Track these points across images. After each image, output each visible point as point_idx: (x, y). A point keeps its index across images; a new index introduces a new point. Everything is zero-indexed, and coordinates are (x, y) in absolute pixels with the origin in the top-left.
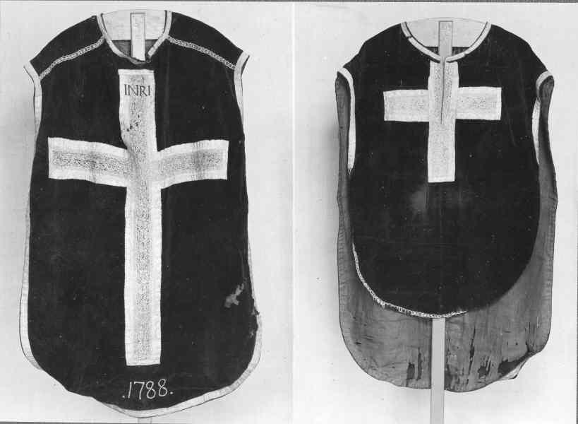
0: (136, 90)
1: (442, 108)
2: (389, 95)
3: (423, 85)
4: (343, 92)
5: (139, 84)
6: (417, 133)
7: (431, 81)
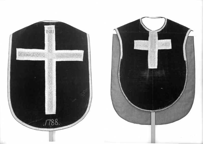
0: (49, 32)
1: (153, 48)
2: (135, 41)
4: (116, 40)
5: (50, 30)
6: (145, 54)
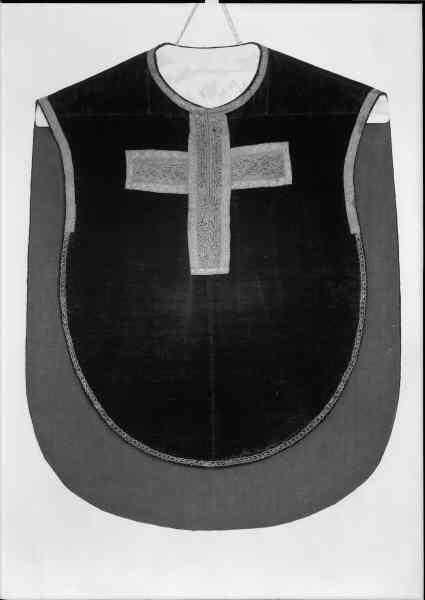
1: (208, 191)
2: (133, 157)
3: (182, 146)
7: (191, 141)
